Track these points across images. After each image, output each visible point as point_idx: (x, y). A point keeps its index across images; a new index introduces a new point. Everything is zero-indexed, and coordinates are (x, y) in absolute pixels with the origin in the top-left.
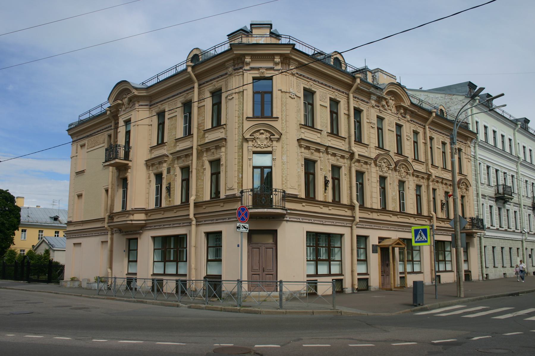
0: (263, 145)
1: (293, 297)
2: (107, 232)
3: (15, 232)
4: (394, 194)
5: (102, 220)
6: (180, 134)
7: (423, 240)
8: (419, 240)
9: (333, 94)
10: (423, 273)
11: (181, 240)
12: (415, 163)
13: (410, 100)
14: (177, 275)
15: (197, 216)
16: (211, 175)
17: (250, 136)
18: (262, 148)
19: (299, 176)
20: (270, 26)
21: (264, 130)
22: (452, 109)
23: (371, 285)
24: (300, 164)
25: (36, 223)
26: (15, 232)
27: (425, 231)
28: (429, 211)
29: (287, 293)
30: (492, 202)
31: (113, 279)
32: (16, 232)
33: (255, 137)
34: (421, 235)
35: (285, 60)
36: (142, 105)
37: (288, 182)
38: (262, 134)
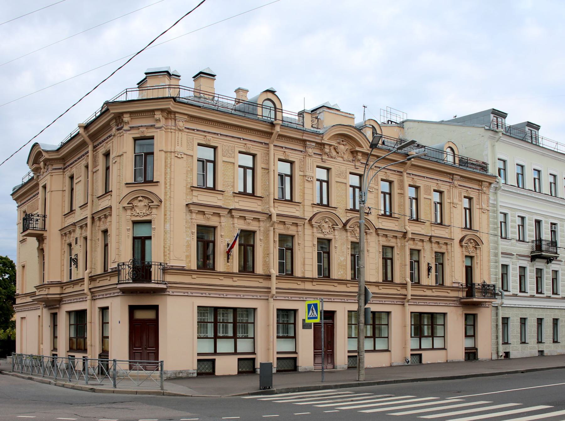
0: (142, 214)
1: (177, 378)
4: (342, 259)
7: (314, 316)
8: (311, 316)
9: (244, 146)
10: (390, 351)
12: (383, 220)
14: (235, 353)
15: (93, 290)
17: (128, 204)
18: (141, 216)
19: (189, 246)
21: (142, 197)
23: (299, 365)
24: (190, 231)
27: (316, 305)
29: (168, 372)
30: (526, 262)
33: (133, 205)
35: (170, 115)
36: (56, 169)
37: (172, 253)
38: (140, 201)
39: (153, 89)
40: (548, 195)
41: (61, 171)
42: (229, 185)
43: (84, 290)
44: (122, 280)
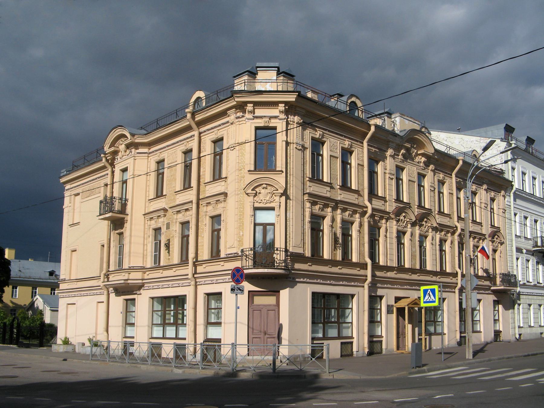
2: (103, 292)
3: (5, 288)
5: (98, 278)
6: (179, 186)
7: (432, 300)
8: (427, 300)
11: (180, 301)
13: (434, 148)
14: (177, 338)
16: (212, 231)
18: (264, 203)
20: (277, 69)
22: (487, 154)
25: (29, 278)
26: (5, 288)
27: (433, 291)
28: (453, 266)
31: (119, 343)
32: (6, 289)
34: (429, 295)
39: (271, 82)
40: (304, 191)
41: (146, 155)
42: (334, 178)
43: (188, 275)
44: (247, 265)
